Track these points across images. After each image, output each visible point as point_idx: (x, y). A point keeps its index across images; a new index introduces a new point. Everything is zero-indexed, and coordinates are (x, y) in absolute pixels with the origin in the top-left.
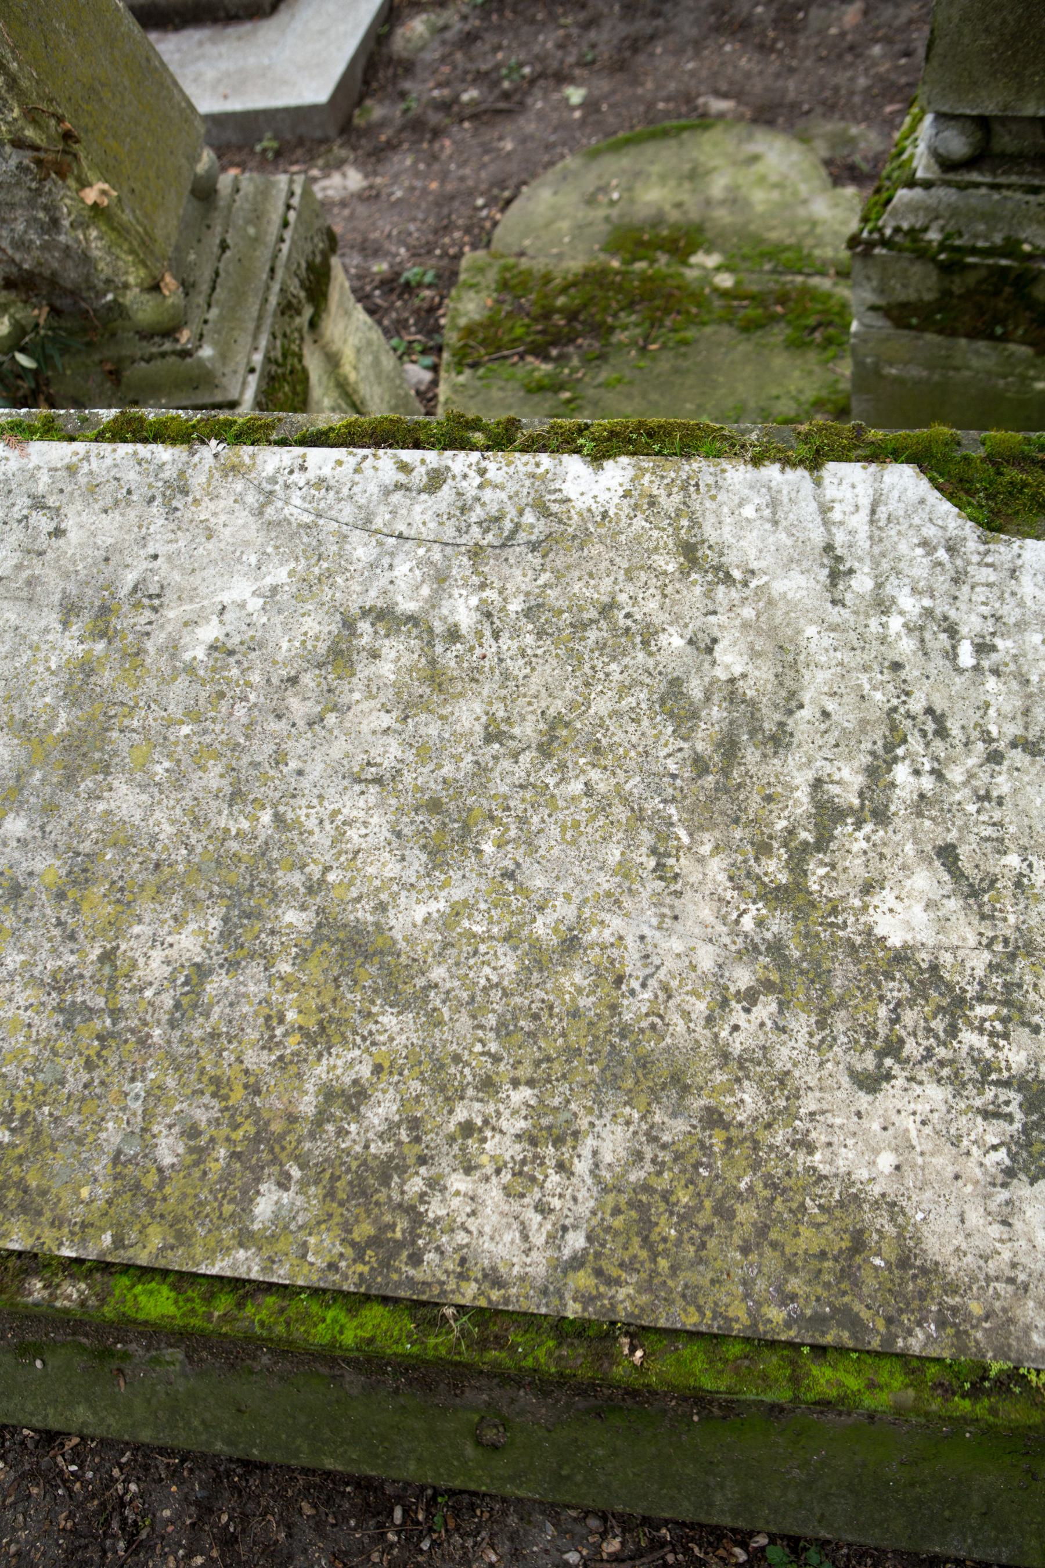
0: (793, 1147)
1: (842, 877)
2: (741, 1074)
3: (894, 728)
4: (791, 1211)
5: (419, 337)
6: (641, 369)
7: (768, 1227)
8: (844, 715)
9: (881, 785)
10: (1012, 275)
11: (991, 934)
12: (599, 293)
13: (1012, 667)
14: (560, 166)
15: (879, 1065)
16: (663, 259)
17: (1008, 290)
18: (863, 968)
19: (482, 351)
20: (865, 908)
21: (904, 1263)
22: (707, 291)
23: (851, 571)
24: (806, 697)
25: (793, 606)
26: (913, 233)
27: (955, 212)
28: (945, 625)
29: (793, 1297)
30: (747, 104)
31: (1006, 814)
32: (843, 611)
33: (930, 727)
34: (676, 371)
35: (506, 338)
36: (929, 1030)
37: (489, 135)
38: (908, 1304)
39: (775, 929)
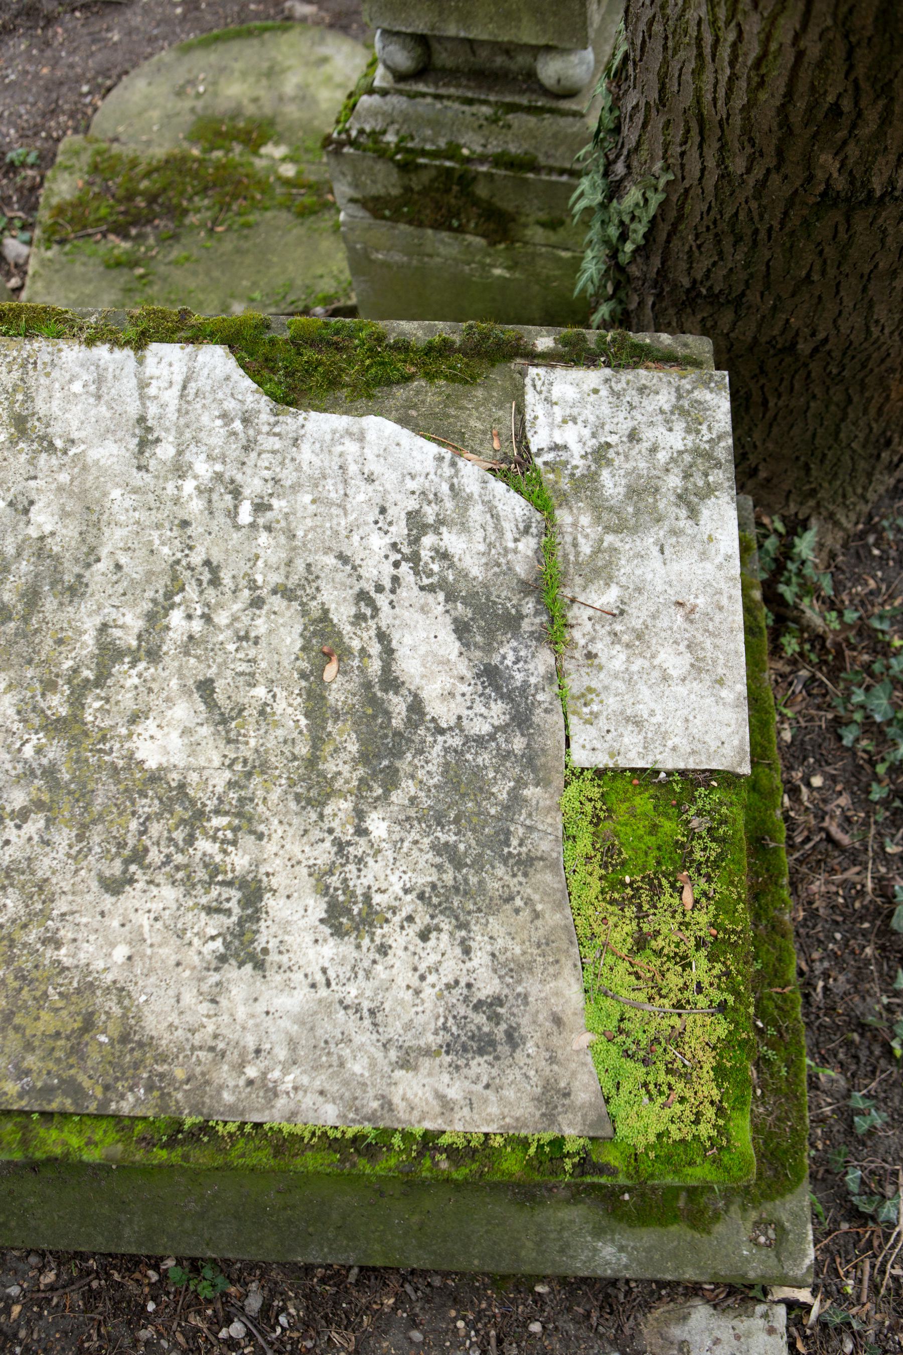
0: (43, 943)
1: (114, 709)
2: (6, 882)
3: (175, 578)
4: (35, 999)
5: (20, 214)
6: (207, 249)
7: (13, 1013)
8: (134, 567)
9: (157, 628)
10: (457, 175)
11: (233, 756)
12: (178, 179)
13: (283, 524)
14: (155, 58)
15: (125, 871)
16: (238, 148)
17: (455, 188)
18: (121, 787)
19: (69, 229)
20: (130, 735)
21: (124, 1039)
22: (272, 179)
23: (158, 440)
24: (104, 552)
25: (103, 471)
26: (375, 135)
27: (407, 118)
28: (231, 487)
29: (28, 1072)
30: (327, 10)
31: (261, 653)
32: (145, 475)
33: (206, 576)
34: (238, 251)
35: (92, 218)
36: (170, 839)
37: (98, 25)
38: (123, 1073)
39: (51, 755)
